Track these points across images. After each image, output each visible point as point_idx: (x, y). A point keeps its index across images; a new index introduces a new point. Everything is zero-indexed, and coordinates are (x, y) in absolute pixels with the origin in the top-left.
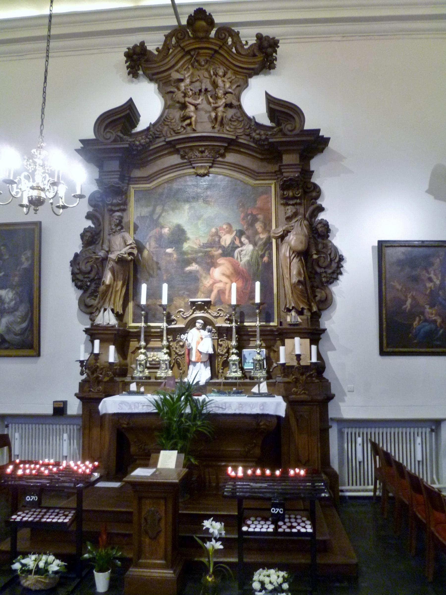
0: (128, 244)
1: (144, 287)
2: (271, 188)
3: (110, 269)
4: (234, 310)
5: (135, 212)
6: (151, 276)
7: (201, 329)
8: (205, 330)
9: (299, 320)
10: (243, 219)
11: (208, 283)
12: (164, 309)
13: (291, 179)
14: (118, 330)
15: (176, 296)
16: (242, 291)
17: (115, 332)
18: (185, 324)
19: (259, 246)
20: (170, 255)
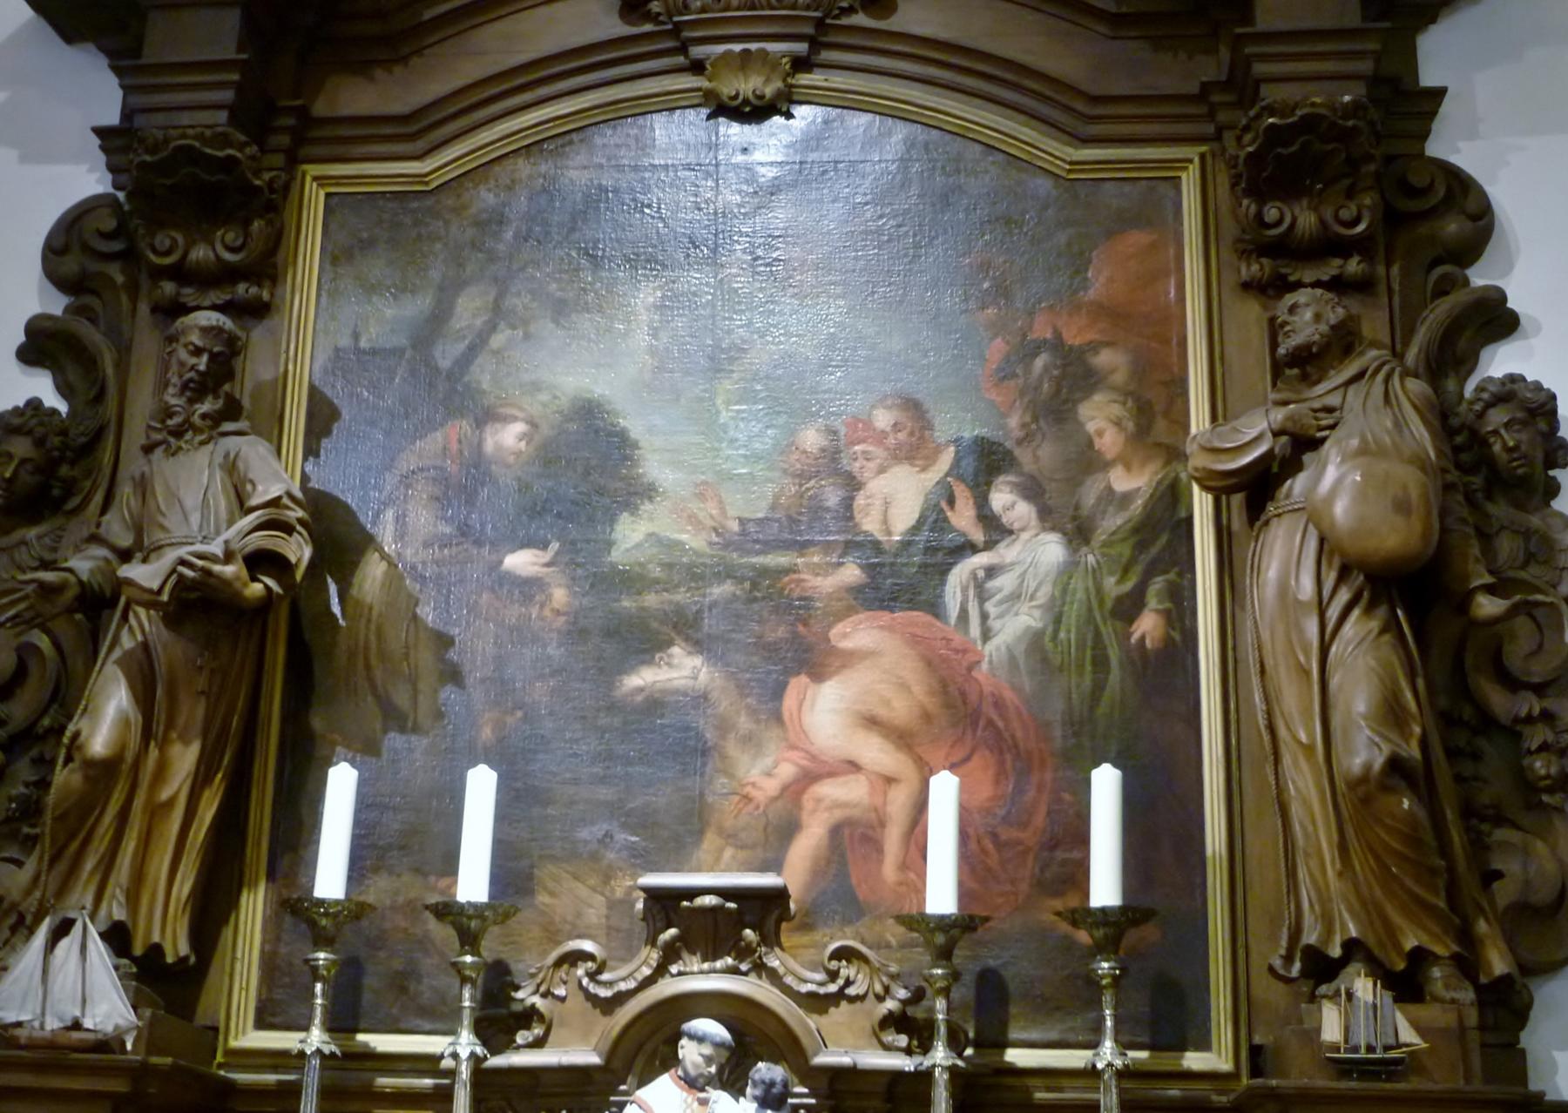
0: (254, 502)
1: (341, 785)
3: (125, 663)
4: (944, 954)
5: (321, 323)
6: (396, 719)
7: (711, 1081)
8: (737, 1090)
10: (1004, 375)
11: (769, 774)
12: (469, 940)
13: (1310, 123)
14: (140, 1073)
15: (553, 859)
16: (994, 836)
17: (119, 1086)
18: (606, 1045)
19: (1105, 544)
20: (528, 587)
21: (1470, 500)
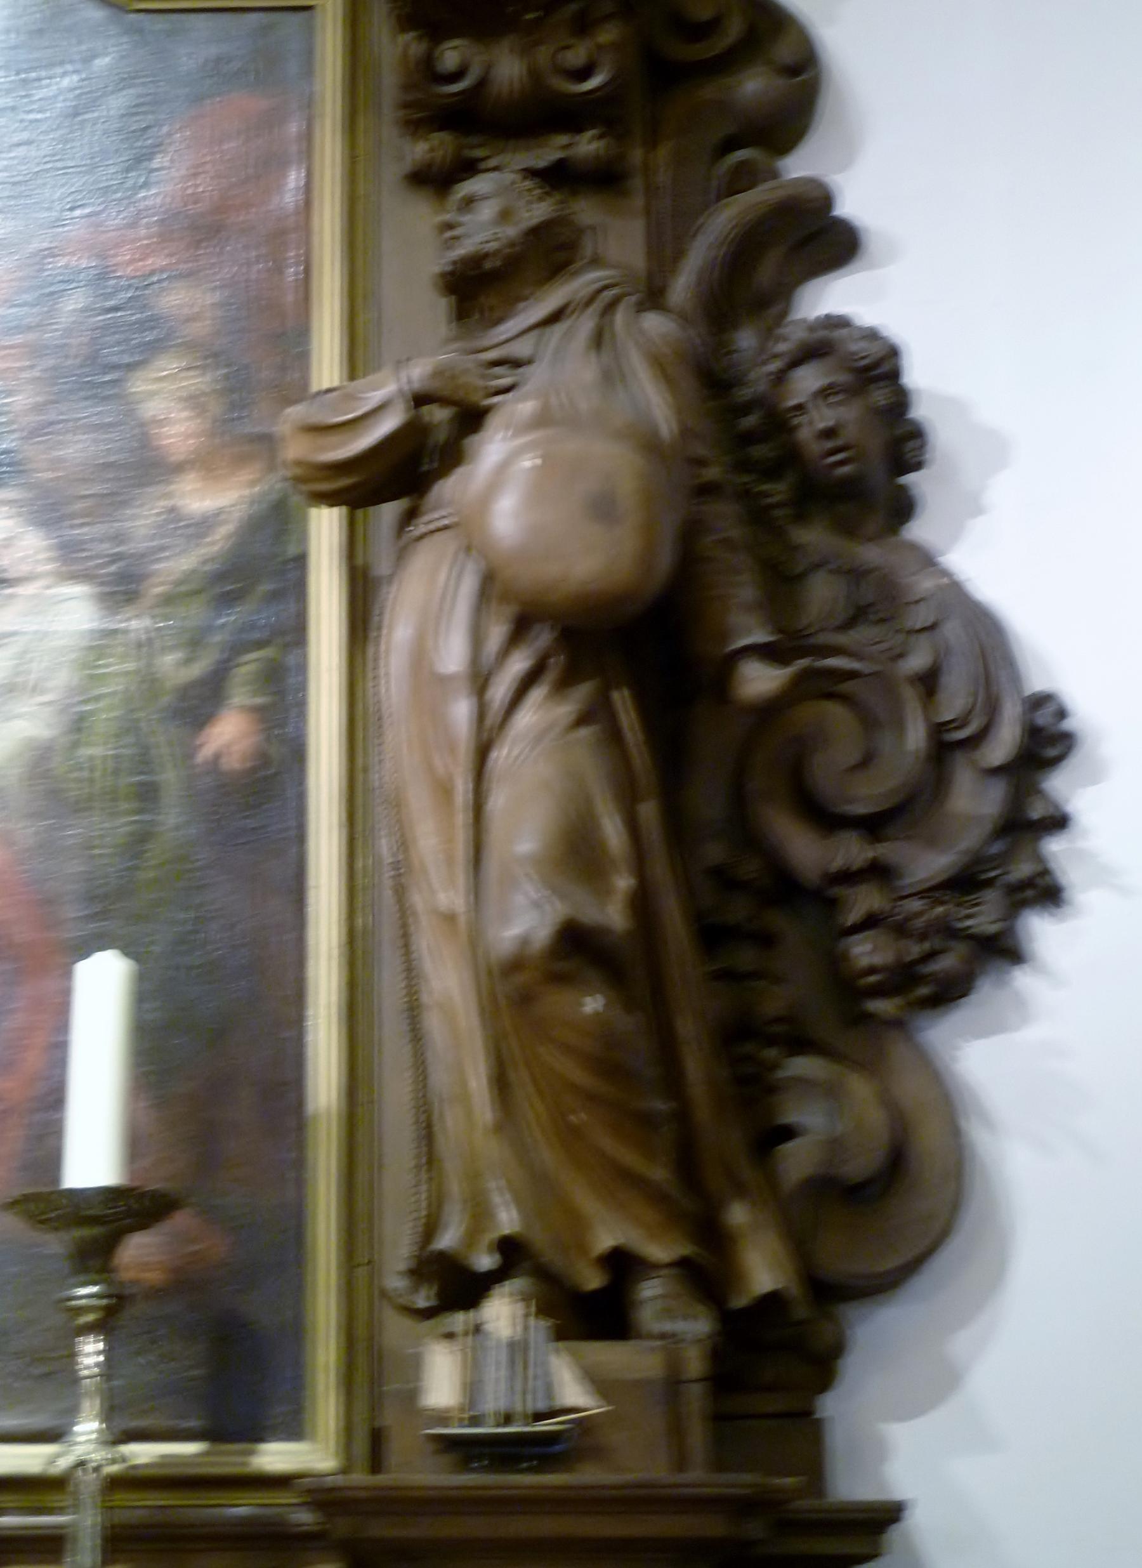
2: (310, 33)
9: (573, 1393)
21: (759, 517)
